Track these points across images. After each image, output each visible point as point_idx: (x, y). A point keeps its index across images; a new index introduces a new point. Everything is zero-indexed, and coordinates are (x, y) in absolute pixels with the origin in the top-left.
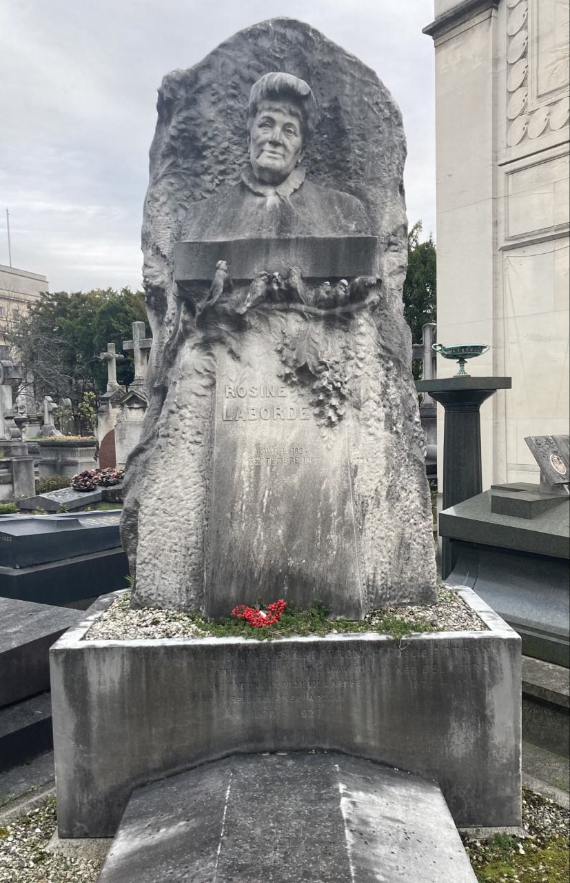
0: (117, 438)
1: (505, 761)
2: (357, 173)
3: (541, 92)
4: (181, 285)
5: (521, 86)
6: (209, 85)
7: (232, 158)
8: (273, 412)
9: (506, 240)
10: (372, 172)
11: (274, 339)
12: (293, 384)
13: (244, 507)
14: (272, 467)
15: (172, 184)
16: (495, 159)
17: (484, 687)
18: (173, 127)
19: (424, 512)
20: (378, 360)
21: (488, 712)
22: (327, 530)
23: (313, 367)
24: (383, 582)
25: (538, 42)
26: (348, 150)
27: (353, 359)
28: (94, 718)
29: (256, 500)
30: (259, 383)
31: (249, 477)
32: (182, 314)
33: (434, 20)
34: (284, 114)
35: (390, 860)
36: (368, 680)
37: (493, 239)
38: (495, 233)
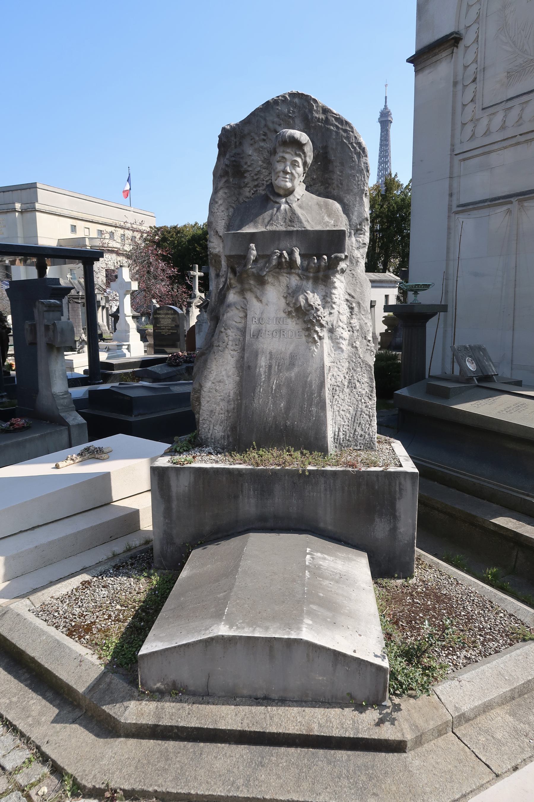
0: (197, 331)
1: (406, 542)
2: (338, 186)
3: (484, 106)
4: (229, 258)
5: (472, 101)
6: (249, 134)
7: (262, 177)
8: (280, 332)
9: (458, 206)
10: (348, 185)
11: (282, 289)
12: (292, 317)
13: (261, 390)
14: (279, 366)
15: (226, 193)
16: (453, 150)
17: (395, 499)
18: (227, 159)
19: (371, 396)
20: (345, 303)
21: (397, 514)
22: (311, 405)
23: (305, 307)
24: (343, 436)
25: (484, 71)
26: (333, 172)
27: (329, 302)
28: (174, 504)
29: (269, 386)
30: (272, 315)
31: (265, 372)
32: (229, 274)
33: (414, 53)
34: (292, 155)
35: (328, 587)
36: (328, 492)
37: (449, 205)
38: (450, 201)
